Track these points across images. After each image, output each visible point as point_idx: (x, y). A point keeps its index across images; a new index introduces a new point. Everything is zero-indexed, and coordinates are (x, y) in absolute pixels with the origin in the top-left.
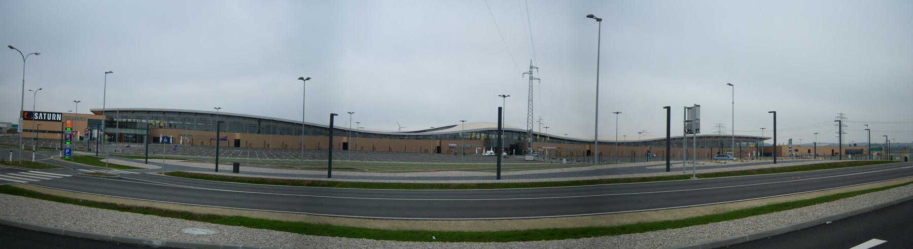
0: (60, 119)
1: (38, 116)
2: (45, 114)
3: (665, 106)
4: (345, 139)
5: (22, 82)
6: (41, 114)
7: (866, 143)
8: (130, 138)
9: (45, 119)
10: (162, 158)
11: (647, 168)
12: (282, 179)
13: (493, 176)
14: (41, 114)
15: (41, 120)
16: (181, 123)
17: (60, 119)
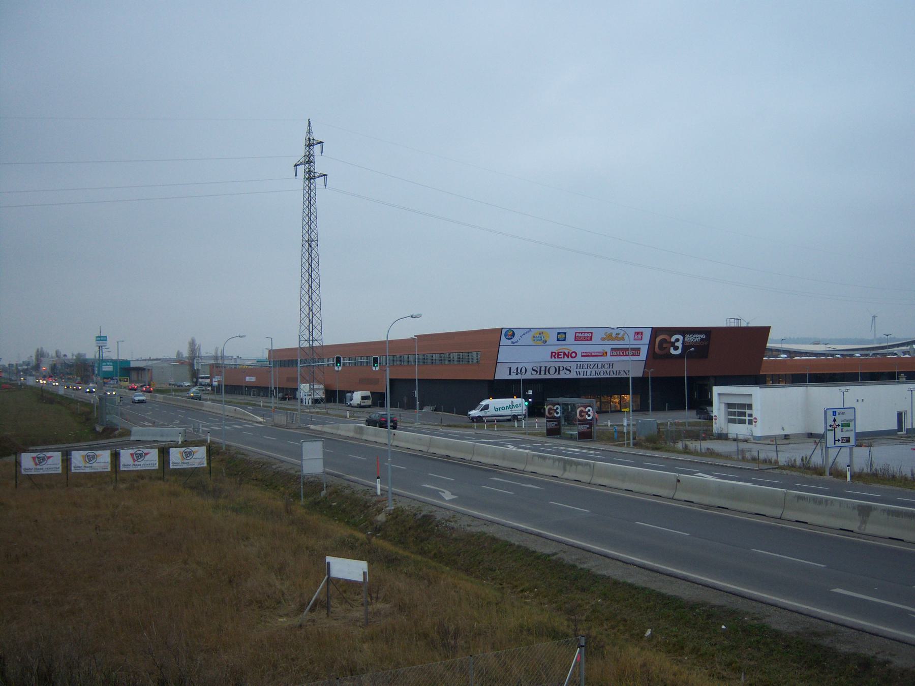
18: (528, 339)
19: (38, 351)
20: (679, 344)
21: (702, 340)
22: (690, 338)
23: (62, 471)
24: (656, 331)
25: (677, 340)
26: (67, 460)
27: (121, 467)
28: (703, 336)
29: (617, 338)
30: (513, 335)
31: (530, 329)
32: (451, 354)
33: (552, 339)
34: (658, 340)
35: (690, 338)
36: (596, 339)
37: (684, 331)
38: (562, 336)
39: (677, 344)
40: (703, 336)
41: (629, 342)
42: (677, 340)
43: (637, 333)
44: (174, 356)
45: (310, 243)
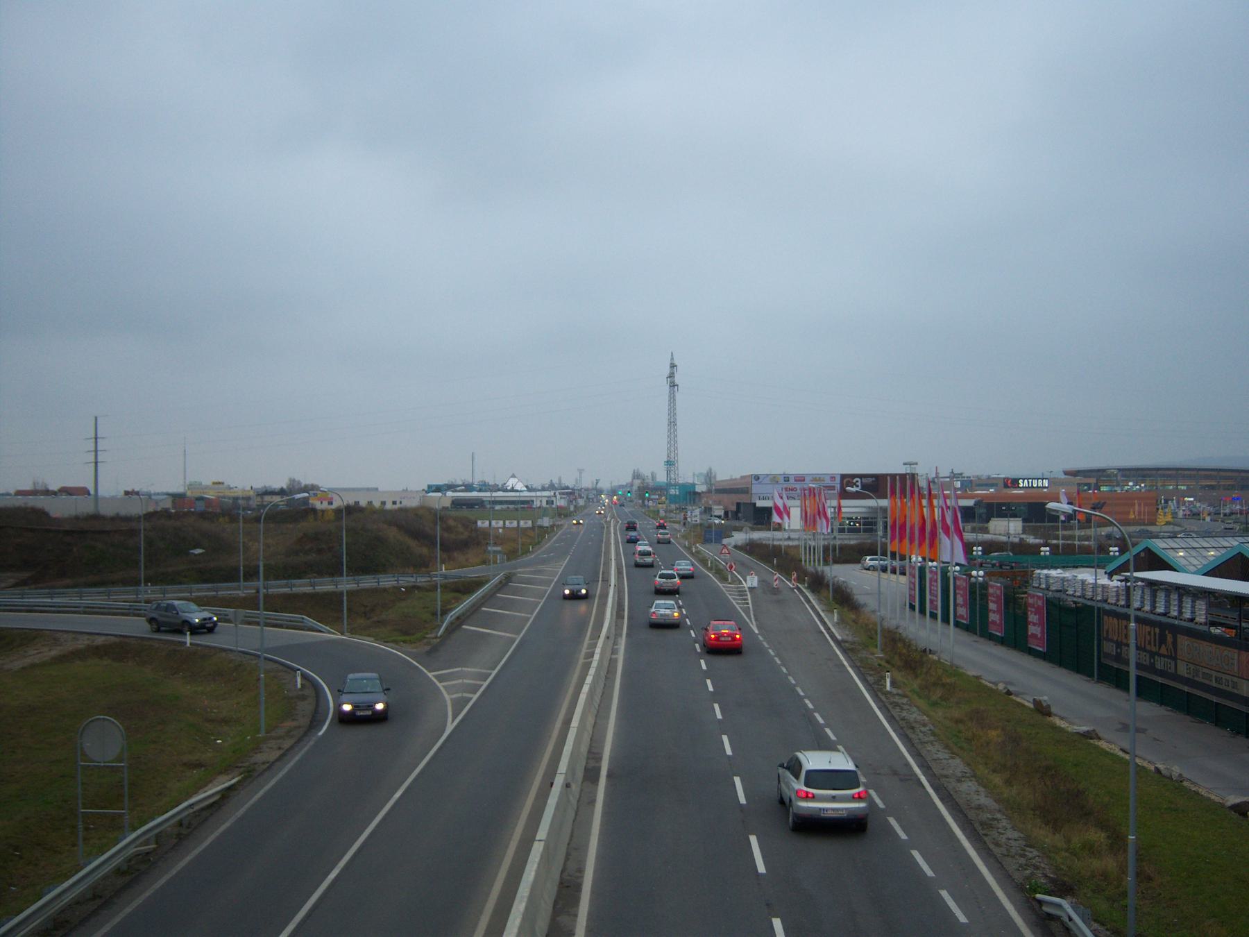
0: (1047, 485)
1: (1023, 483)
2: (1030, 481)
3: (906, 461)
4: (540, 499)
5: (94, 421)
6: (1026, 481)
7: (664, 482)
8: (246, 521)
9: (1030, 485)
10: (258, 624)
11: (519, 575)
12: (603, 816)
13: (835, 637)
14: (1026, 481)
15: (1026, 487)
16: (1143, 485)
17: (1047, 485)
18: (767, 480)
19: (634, 472)
20: (859, 484)
21: (873, 481)
22: (865, 480)
23: (758, 584)
24: (843, 477)
25: (857, 482)
26: (518, 523)
27: (528, 526)
28: (874, 479)
29: (820, 480)
30: (758, 478)
31: (768, 475)
32: (1030, 481)
33: (781, 480)
34: (845, 481)
35: (865, 480)
36: (808, 479)
37: (861, 476)
38: (787, 479)
39: (857, 484)
40: (874, 479)
41: (828, 482)
42: (857, 482)
43: (832, 477)
44: (626, 479)
45: (672, 423)
